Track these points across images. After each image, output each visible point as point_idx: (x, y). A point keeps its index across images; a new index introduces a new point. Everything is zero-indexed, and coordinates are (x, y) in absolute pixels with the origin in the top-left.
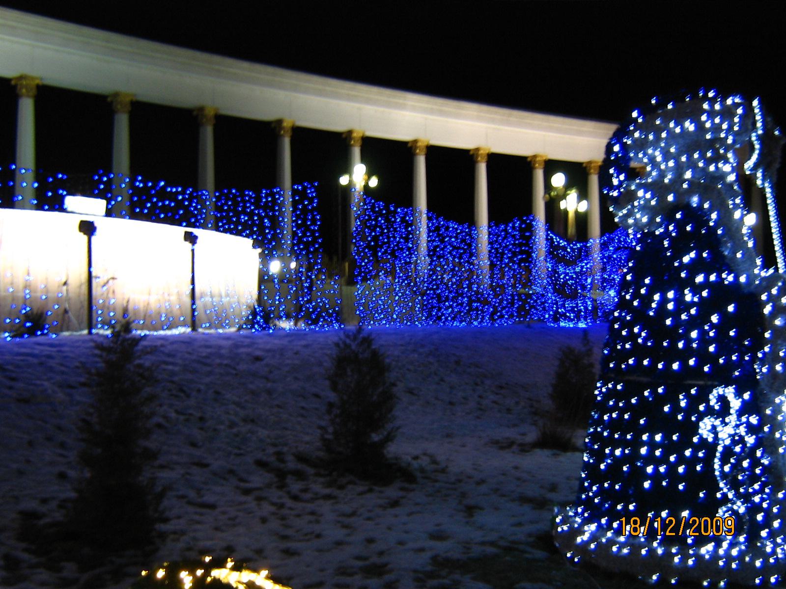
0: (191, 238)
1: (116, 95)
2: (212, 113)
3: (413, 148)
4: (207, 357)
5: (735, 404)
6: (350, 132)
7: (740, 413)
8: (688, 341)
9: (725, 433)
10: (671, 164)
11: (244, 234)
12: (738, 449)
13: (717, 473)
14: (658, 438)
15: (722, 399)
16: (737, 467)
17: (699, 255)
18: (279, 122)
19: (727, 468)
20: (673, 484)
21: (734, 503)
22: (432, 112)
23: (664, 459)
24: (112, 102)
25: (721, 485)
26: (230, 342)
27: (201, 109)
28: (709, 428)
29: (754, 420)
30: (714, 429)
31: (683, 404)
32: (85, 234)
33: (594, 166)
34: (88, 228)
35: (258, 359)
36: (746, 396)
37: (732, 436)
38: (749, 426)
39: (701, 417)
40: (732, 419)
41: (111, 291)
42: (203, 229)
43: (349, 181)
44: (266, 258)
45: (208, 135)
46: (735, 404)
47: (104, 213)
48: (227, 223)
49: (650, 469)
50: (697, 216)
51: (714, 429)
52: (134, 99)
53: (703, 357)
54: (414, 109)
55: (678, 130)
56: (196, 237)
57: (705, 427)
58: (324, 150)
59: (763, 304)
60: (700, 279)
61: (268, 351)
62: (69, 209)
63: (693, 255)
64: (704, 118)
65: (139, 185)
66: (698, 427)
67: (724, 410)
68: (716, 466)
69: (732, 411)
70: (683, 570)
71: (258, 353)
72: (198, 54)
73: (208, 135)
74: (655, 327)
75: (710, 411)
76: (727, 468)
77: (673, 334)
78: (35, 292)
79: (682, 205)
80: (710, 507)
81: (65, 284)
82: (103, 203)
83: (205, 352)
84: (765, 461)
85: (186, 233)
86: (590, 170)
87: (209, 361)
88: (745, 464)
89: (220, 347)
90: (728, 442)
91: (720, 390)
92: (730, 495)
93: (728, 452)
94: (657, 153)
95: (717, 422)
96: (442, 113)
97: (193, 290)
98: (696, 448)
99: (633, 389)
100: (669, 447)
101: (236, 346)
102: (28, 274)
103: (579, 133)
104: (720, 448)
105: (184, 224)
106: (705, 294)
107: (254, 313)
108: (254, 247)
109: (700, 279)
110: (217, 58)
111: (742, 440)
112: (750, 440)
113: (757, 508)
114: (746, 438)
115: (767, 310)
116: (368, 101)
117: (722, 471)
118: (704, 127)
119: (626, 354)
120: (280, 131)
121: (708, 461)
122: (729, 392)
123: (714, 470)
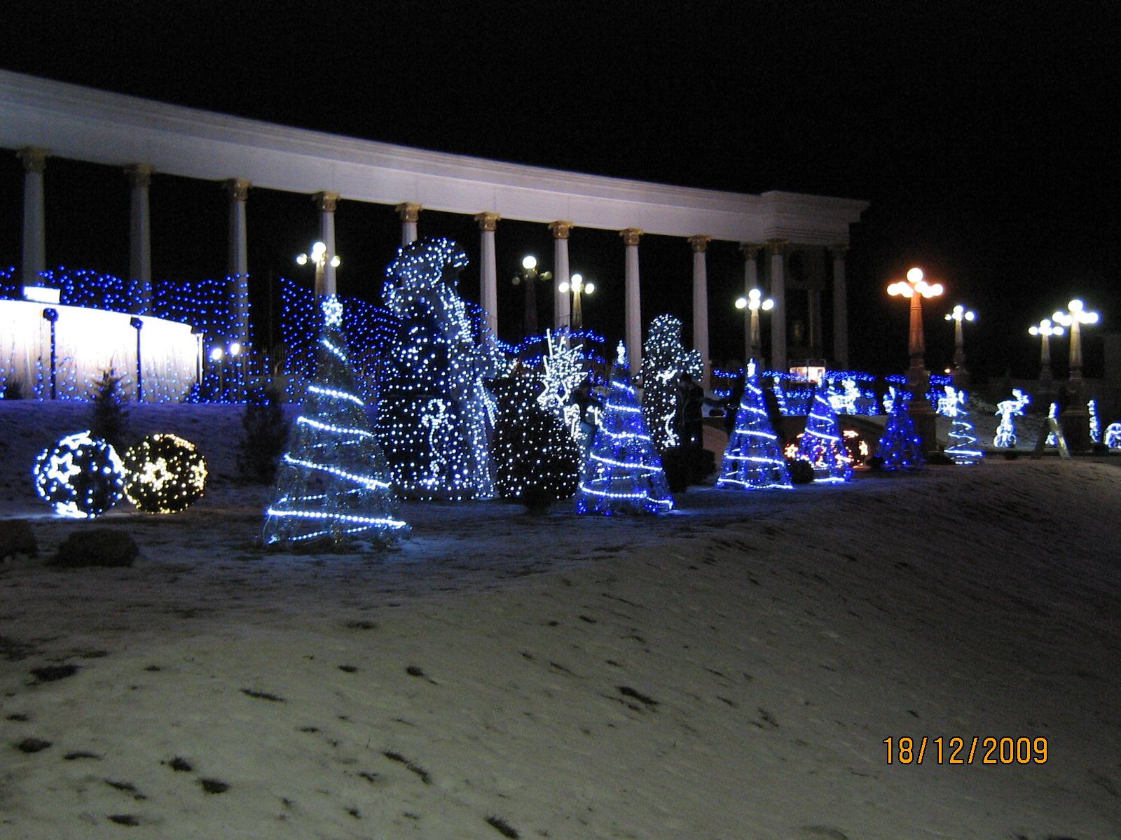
0: (136, 323)
1: (27, 150)
2: (148, 172)
3: (402, 214)
4: (153, 418)
5: (443, 408)
6: (321, 194)
7: (444, 413)
8: (417, 375)
9: (436, 423)
10: (415, 279)
11: (163, 316)
12: (443, 431)
13: (431, 443)
14: (401, 426)
15: (435, 405)
16: (442, 441)
17: (420, 328)
18: (232, 182)
19: (436, 441)
20: (408, 450)
21: (441, 459)
22: (425, 169)
23: (403, 437)
24: (21, 159)
25: (433, 449)
26: (171, 409)
27: (133, 167)
28: (427, 419)
29: (454, 417)
30: (430, 421)
31: (414, 408)
32: (48, 319)
33: (633, 235)
34: (50, 315)
35: (195, 421)
36: (449, 404)
37: (440, 425)
38: (450, 420)
39: (423, 414)
40: (441, 415)
41: (74, 365)
42: (16, 300)
43: (308, 260)
44: (207, 346)
45: (142, 197)
46: (443, 408)
47: (58, 301)
48: (166, 309)
49: (396, 442)
50: (422, 308)
51: (430, 421)
52: (50, 155)
53: (424, 382)
54: (401, 166)
55: (415, 262)
56: (141, 323)
57: (425, 419)
58: (288, 215)
59: (448, 353)
60: (419, 341)
61: (204, 416)
62: (29, 298)
63: (416, 329)
64: (427, 256)
65: (227, 357)
66: (421, 420)
67: (436, 410)
68: (431, 440)
69: (440, 411)
70: (409, 492)
71: (196, 417)
72: (131, 100)
73: (142, 197)
74: (401, 367)
75: (428, 412)
76: (436, 441)
77: (410, 371)
78: (17, 368)
79: (416, 303)
80: (426, 462)
81: (40, 359)
82: (57, 293)
83: (152, 414)
84: (461, 439)
85: (132, 319)
86: (628, 240)
87: (154, 420)
88: (447, 439)
89: (164, 412)
90: (438, 427)
91: (435, 401)
92: (438, 455)
93: (437, 433)
94: (409, 273)
95: (432, 417)
96: (437, 171)
97: (139, 373)
98: (419, 431)
99: (391, 402)
100: (405, 430)
101: (177, 412)
102: (13, 348)
103: (612, 195)
104: (433, 430)
105: (125, 310)
106: (421, 349)
107: (193, 390)
108: (193, 332)
109: (419, 341)
110: (153, 105)
111: (446, 428)
112: (451, 427)
113: (455, 462)
114: (449, 426)
115: (449, 356)
116: (344, 156)
117: (434, 443)
118: (428, 260)
119: (390, 383)
120: (233, 193)
121: (426, 438)
122: (440, 402)
123: (429, 442)
